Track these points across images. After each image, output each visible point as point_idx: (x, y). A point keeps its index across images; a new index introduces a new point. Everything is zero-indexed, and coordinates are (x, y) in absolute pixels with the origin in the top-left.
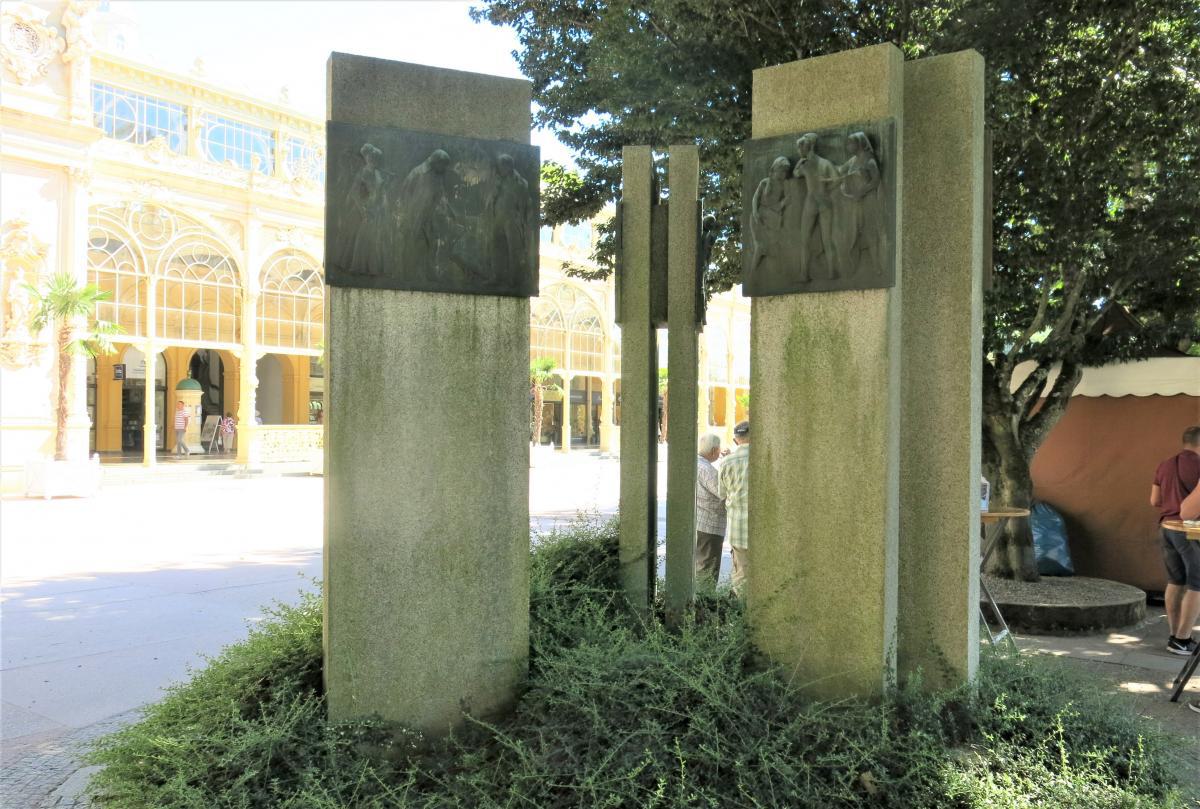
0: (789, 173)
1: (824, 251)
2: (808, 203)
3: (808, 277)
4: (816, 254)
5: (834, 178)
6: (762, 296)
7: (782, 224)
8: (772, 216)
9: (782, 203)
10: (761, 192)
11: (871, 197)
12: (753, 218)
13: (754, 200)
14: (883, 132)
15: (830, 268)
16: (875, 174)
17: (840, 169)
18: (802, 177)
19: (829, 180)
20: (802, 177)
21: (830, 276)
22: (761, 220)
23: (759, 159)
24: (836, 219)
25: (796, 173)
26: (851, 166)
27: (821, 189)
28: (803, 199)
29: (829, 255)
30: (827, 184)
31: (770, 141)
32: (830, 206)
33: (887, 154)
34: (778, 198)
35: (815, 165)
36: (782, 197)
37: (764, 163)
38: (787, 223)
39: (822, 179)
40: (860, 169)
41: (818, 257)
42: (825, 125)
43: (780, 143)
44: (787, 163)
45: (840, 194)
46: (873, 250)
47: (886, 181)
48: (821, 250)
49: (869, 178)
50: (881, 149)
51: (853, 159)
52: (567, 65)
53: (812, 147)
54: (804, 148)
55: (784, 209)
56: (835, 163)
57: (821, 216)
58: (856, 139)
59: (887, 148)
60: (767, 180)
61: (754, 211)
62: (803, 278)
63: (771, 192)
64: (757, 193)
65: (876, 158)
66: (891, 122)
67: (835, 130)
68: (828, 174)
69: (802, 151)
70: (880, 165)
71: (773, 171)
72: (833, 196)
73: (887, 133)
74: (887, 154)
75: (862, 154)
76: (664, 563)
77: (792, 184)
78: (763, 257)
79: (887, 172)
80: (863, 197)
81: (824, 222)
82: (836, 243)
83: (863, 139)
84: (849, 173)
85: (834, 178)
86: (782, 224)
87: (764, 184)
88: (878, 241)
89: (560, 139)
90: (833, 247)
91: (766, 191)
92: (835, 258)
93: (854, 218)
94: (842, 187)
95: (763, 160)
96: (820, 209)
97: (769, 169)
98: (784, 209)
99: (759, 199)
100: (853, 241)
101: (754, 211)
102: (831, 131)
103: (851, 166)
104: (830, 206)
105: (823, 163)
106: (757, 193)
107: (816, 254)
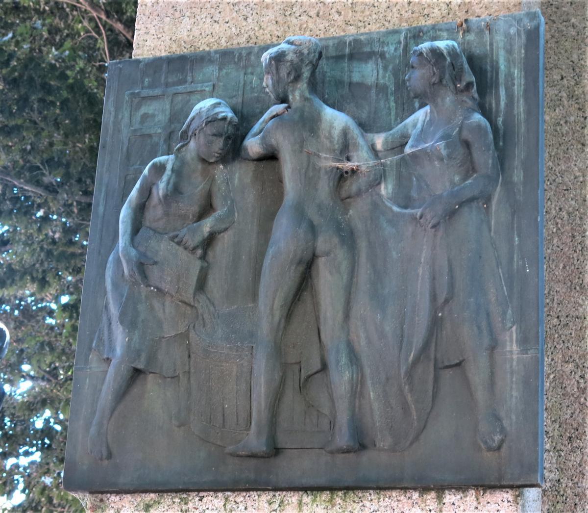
0: (233, 148)
1: (324, 367)
2: (283, 225)
3: (272, 438)
4: (299, 375)
5: (361, 160)
6: (121, 492)
7: (201, 285)
8: (175, 262)
9: (207, 225)
10: (147, 192)
11: (469, 219)
12: (118, 261)
13: (125, 213)
14: (509, 52)
15: (343, 418)
16: (485, 158)
17: (379, 140)
18: (270, 157)
19: (348, 165)
20: (270, 157)
21: (343, 439)
22: (142, 267)
23: (148, 108)
24: (364, 274)
25: (253, 145)
26: (414, 133)
27: (324, 188)
28: (268, 217)
29: (341, 378)
30: (342, 177)
31: (180, 66)
32: (348, 238)
33: (520, 108)
34: (195, 209)
35: (309, 123)
36: (207, 208)
37: (162, 118)
38: (215, 284)
39: (328, 162)
40: (446, 137)
41: (304, 385)
42: (335, 32)
43: (211, 71)
44: (226, 112)
45: (377, 206)
46: (478, 374)
47: (518, 176)
48: (316, 365)
49: (470, 168)
50: (502, 93)
51: (421, 115)
52: (45, 488)
53: (306, 73)
54: (284, 72)
55: (209, 241)
56: (365, 127)
57: (321, 262)
58: (436, 53)
59: (518, 88)
60: (168, 160)
61: (122, 241)
62: (255, 441)
63: (176, 191)
64: (134, 193)
65: (486, 112)
66: (529, 25)
67: (370, 42)
68: (345, 149)
69: (277, 82)
70: (502, 139)
71: (185, 137)
72: (357, 212)
73: (519, 52)
74: (520, 108)
75: (448, 99)
76: (522, 101)
77: (238, 177)
78: (137, 373)
79: (519, 154)
80: (451, 214)
81: (328, 283)
82: (361, 344)
83: (453, 53)
84: (408, 150)
85: (361, 160)
86: (201, 285)
87: (159, 169)
88: (494, 346)
89: (10, 500)
90: (354, 357)
91: (161, 188)
92: (357, 390)
93: (423, 271)
94: (386, 190)
95: (158, 111)
96: (322, 244)
97: (175, 134)
98: (209, 241)
99: (141, 209)
100: (418, 341)
101: (122, 241)
102: (357, 43)
103: (414, 133)
104: (348, 238)
105: (335, 119)
106: (134, 193)
107: (299, 375)
